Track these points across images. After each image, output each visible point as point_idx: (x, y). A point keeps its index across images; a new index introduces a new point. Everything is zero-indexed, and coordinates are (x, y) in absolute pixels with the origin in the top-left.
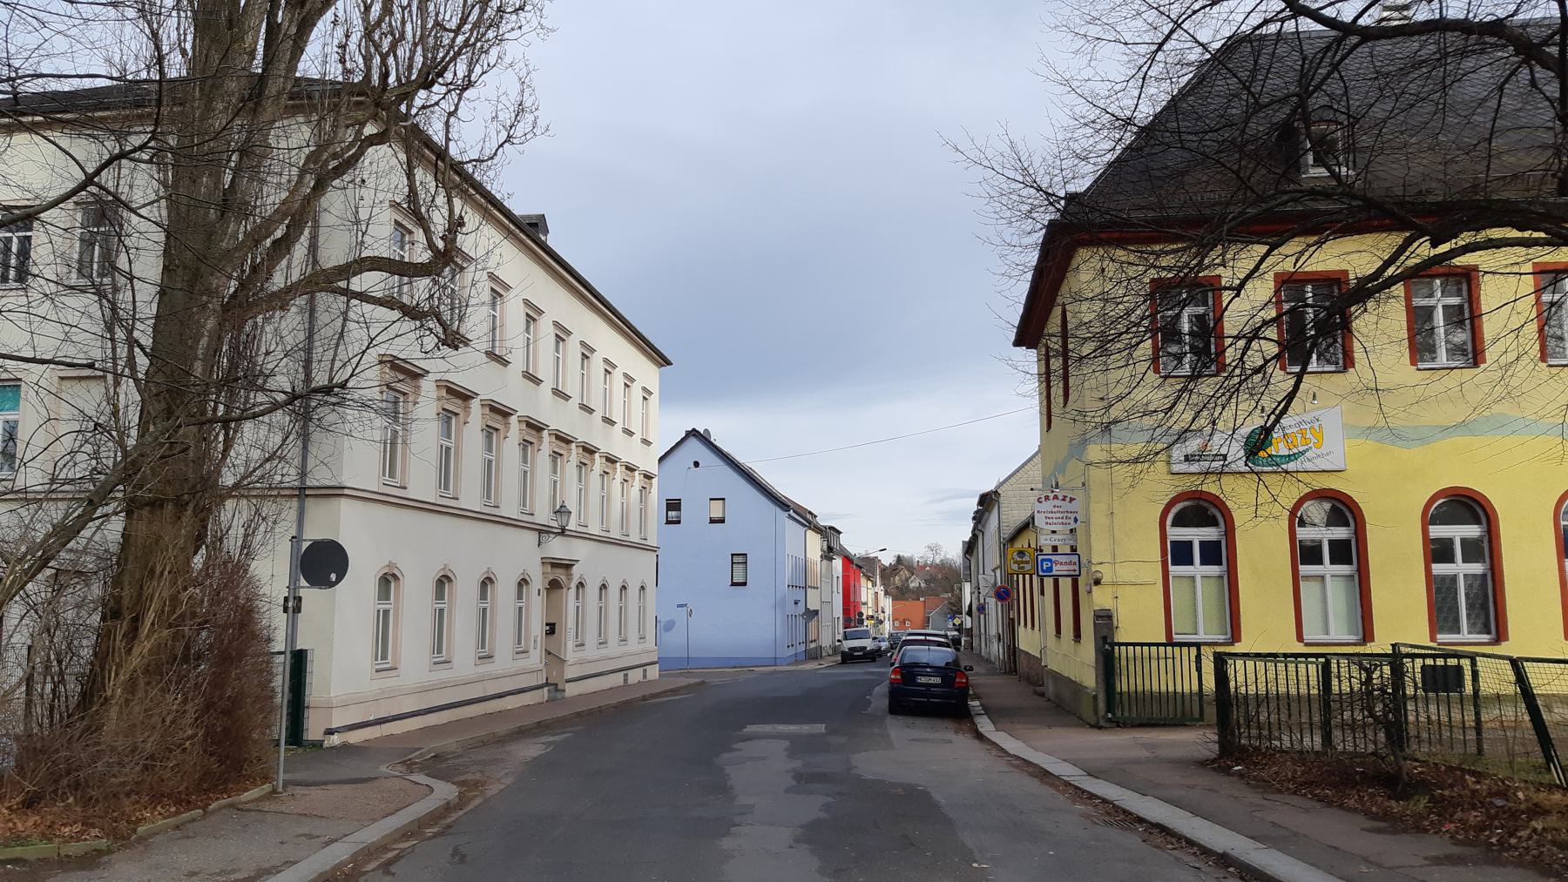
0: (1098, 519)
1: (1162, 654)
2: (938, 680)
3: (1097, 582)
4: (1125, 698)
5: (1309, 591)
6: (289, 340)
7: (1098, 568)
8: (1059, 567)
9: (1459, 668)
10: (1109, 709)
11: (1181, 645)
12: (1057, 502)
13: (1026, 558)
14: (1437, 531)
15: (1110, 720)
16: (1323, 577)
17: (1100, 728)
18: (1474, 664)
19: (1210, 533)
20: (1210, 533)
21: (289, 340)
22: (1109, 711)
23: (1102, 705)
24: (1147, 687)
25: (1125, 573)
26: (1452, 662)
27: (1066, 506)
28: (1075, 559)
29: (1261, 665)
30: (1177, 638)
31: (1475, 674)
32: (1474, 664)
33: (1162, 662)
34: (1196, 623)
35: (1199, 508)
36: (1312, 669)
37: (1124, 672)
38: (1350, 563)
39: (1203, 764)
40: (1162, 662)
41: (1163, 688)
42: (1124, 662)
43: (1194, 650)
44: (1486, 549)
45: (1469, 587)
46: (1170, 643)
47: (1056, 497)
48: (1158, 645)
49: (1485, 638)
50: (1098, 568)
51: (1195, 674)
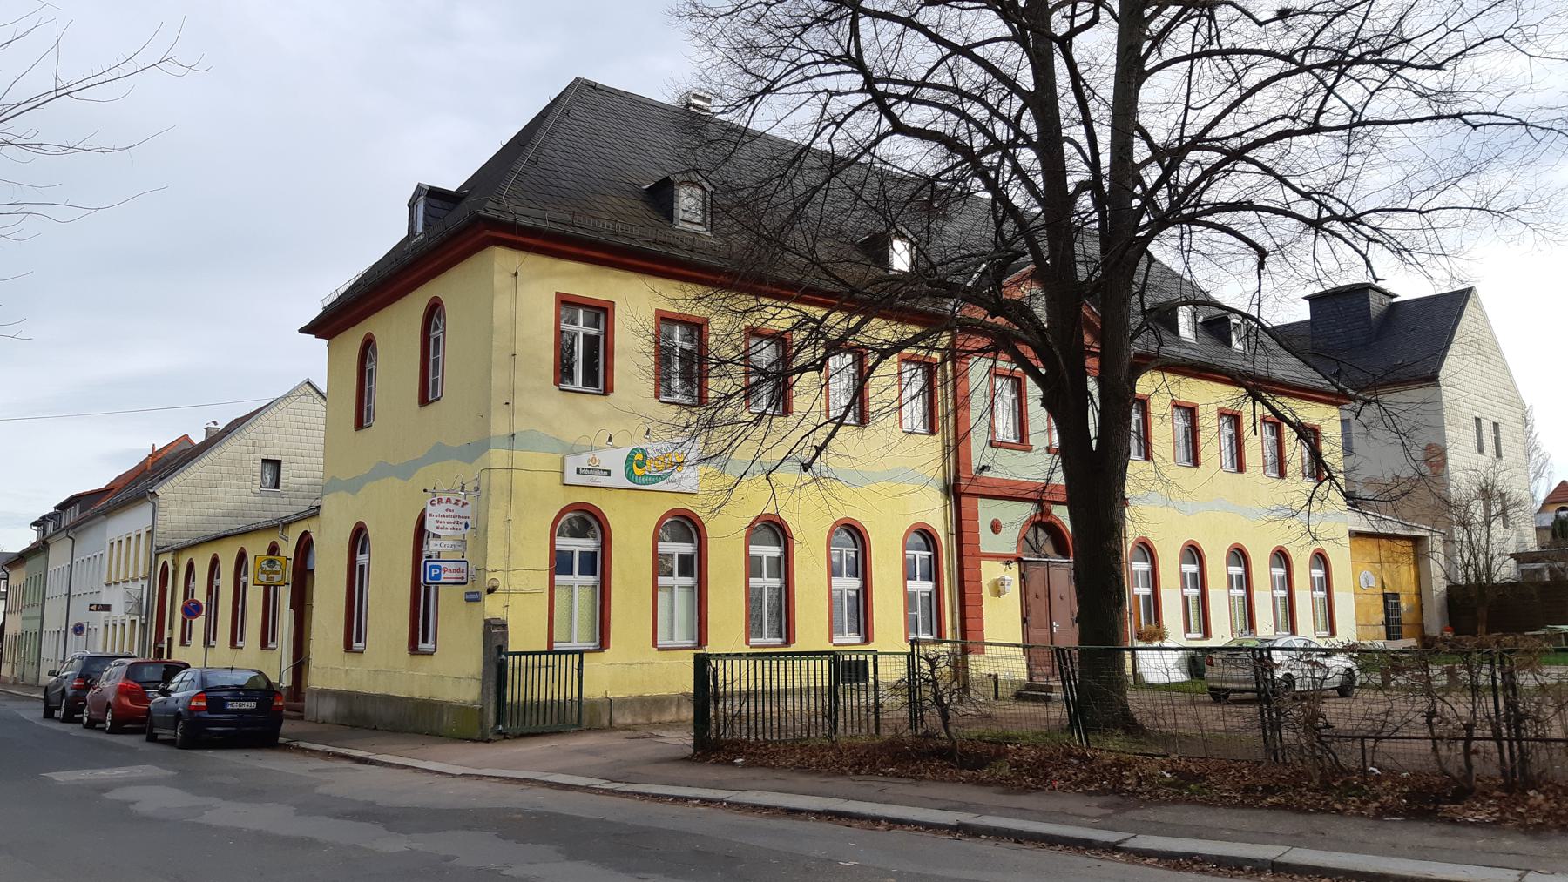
0: (495, 526)
1: (543, 663)
2: (252, 705)
3: (491, 591)
4: (508, 708)
5: (663, 597)
6: (832, 414)
7: (493, 575)
8: (447, 574)
9: (866, 662)
10: (498, 721)
11: (560, 653)
12: (449, 506)
13: (277, 568)
14: (564, 543)
15: (500, 732)
16: (672, 588)
17: (488, 741)
18: (875, 659)
19: (589, 544)
20: (589, 544)
21: (832, 414)
22: (498, 722)
23: (491, 717)
24: (542, 697)
25: (516, 581)
26: (862, 657)
27: (459, 510)
28: (463, 566)
29: (736, 662)
30: (557, 646)
31: (876, 667)
32: (875, 659)
33: (543, 670)
34: (571, 630)
35: (586, 520)
36: (826, 663)
37: (509, 682)
38: (594, 573)
39: (687, 760)
40: (543, 670)
41: (542, 697)
42: (510, 673)
43: (577, 657)
44: (784, 566)
45: (770, 597)
46: (551, 651)
47: (448, 501)
48: (540, 653)
49: (778, 641)
50: (493, 575)
51: (576, 680)
